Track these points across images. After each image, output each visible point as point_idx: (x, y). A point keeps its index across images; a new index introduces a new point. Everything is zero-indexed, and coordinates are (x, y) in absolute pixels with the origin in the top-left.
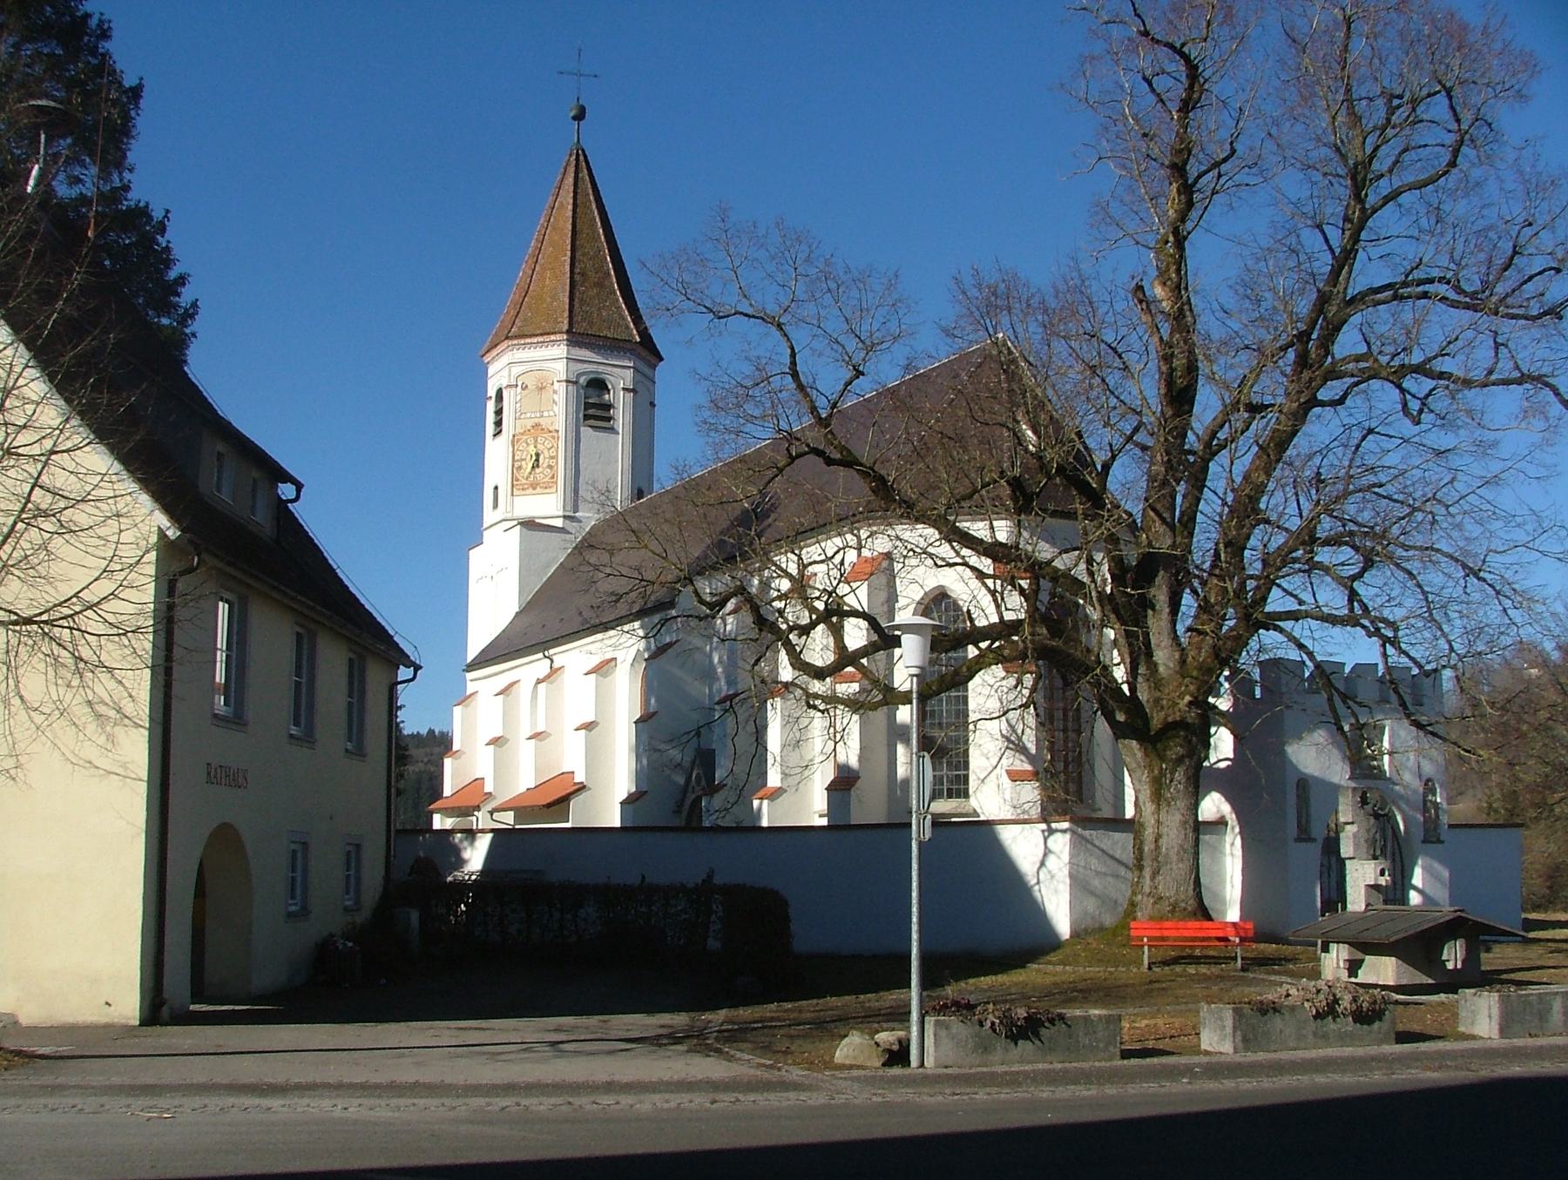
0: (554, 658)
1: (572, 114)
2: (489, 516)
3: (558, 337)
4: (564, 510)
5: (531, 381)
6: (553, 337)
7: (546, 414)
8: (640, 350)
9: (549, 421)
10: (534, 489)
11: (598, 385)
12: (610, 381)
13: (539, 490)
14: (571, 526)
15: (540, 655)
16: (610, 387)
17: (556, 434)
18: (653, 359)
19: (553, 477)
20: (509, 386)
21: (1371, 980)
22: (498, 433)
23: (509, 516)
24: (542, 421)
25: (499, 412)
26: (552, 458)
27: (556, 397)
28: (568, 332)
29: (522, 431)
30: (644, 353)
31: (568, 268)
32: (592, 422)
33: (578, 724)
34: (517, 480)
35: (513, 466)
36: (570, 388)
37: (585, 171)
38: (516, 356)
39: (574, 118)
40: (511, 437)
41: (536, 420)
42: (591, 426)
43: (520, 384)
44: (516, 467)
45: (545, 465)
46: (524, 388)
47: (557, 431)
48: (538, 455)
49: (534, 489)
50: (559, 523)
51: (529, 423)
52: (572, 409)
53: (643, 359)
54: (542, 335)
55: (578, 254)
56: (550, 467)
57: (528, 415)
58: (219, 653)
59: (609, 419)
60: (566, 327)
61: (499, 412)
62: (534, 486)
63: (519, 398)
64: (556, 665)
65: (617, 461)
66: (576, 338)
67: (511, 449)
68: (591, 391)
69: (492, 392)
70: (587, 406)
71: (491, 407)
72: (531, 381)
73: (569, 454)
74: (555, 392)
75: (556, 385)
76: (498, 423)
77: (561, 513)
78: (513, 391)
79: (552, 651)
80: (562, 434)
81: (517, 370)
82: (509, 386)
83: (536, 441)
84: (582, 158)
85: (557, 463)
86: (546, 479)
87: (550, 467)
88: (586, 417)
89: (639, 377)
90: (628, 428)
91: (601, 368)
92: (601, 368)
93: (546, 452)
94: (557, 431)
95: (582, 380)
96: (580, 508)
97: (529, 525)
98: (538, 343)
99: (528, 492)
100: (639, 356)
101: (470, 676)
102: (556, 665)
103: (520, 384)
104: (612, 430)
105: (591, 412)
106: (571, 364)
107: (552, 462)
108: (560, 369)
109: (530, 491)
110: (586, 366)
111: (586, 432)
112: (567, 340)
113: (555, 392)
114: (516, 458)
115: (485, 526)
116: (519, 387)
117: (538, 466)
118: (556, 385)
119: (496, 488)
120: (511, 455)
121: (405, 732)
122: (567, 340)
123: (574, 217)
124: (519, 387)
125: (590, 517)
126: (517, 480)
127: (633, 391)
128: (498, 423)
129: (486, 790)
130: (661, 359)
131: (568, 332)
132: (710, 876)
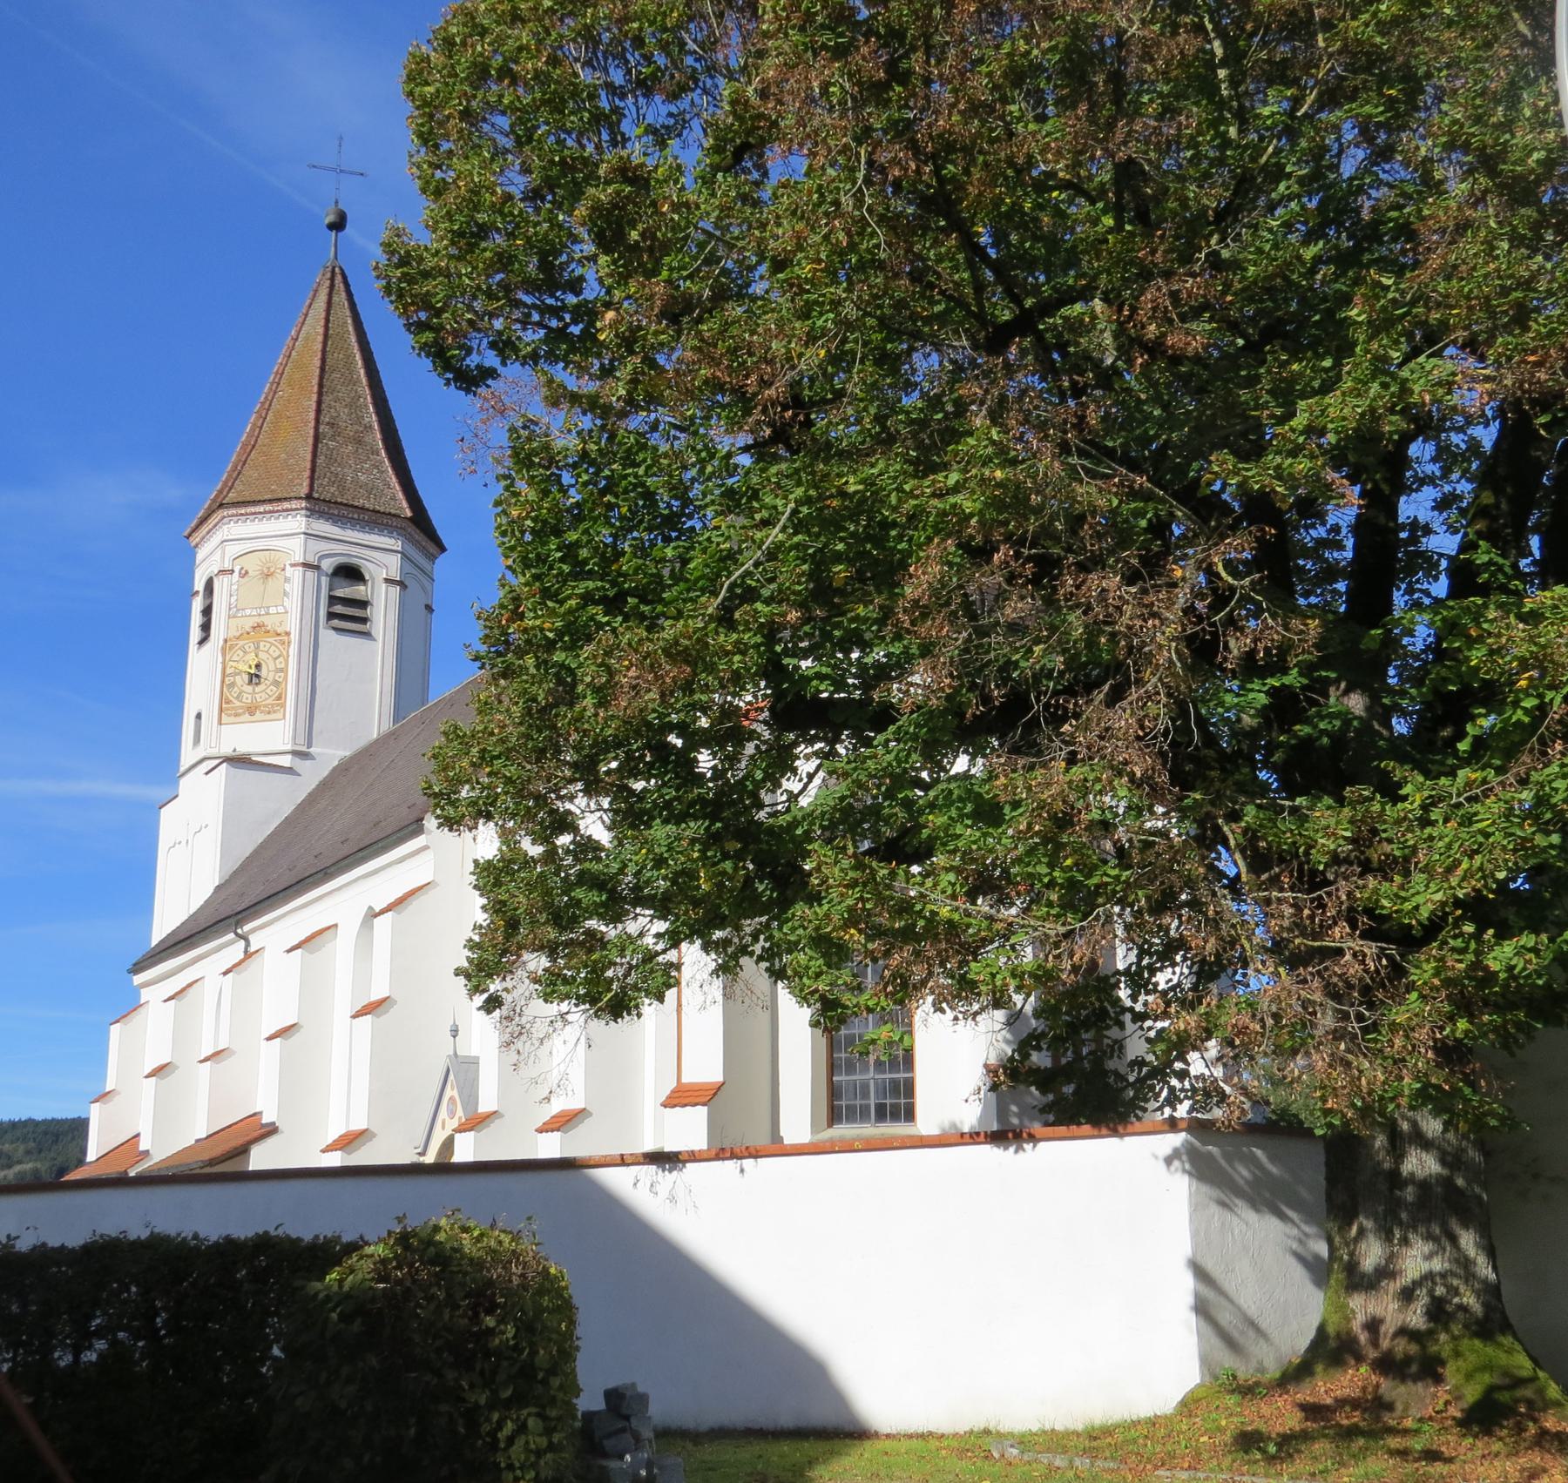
0: (251, 938)
1: (327, 221)
2: (188, 755)
3: (294, 504)
5: (252, 564)
6: (286, 505)
8: (411, 529)
10: (252, 714)
11: (350, 573)
12: (368, 569)
13: (258, 715)
14: (300, 765)
15: (231, 936)
18: (432, 548)
19: (279, 698)
20: (222, 572)
22: (202, 642)
24: (268, 621)
25: (207, 611)
26: (281, 670)
27: (287, 587)
28: (309, 497)
30: (419, 536)
31: (312, 415)
32: (336, 623)
33: (495, 1125)
34: (228, 702)
35: (223, 682)
37: (343, 295)
39: (331, 227)
42: (335, 629)
43: (237, 569)
44: (226, 683)
46: (244, 574)
47: (288, 634)
49: (252, 714)
50: (286, 761)
51: (248, 624)
53: (416, 544)
54: (270, 501)
55: (327, 399)
56: (276, 683)
57: (248, 612)
59: (364, 620)
60: (304, 491)
61: (207, 611)
62: (251, 710)
64: (252, 949)
66: (320, 505)
67: (220, 659)
68: (338, 581)
69: (199, 585)
70: (333, 600)
71: (197, 605)
72: (252, 564)
74: (287, 580)
76: (206, 627)
77: (289, 747)
78: (226, 579)
79: (247, 928)
80: (294, 637)
81: (233, 549)
82: (222, 572)
83: (257, 648)
84: (339, 278)
85: (286, 678)
87: (276, 683)
88: (331, 616)
89: (409, 568)
91: (355, 550)
92: (355, 550)
93: (271, 663)
94: (288, 634)
95: (328, 565)
97: (239, 761)
99: (243, 718)
100: (409, 539)
101: (138, 979)
102: (252, 949)
103: (237, 569)
104: (367, 635)
105: (339, 609)
106: (312, 543)
107: (279, 677)
108: (296, 549)
109: (247, 717)
111: (328, 637)
113: (287, 580)
114: (229, 671)
115: (182, 769)
116: (236, 574)
119: (199, 716)
120: (220, 666)
121: (705, 1147)
123: (324, 351)
124: (236, 574)
125: (330, 754)
127: (401, 584)
128: (206, 627)
129: (142, 1148)
130: (443, 549)
131: (309, 497)
132: (458, 972)
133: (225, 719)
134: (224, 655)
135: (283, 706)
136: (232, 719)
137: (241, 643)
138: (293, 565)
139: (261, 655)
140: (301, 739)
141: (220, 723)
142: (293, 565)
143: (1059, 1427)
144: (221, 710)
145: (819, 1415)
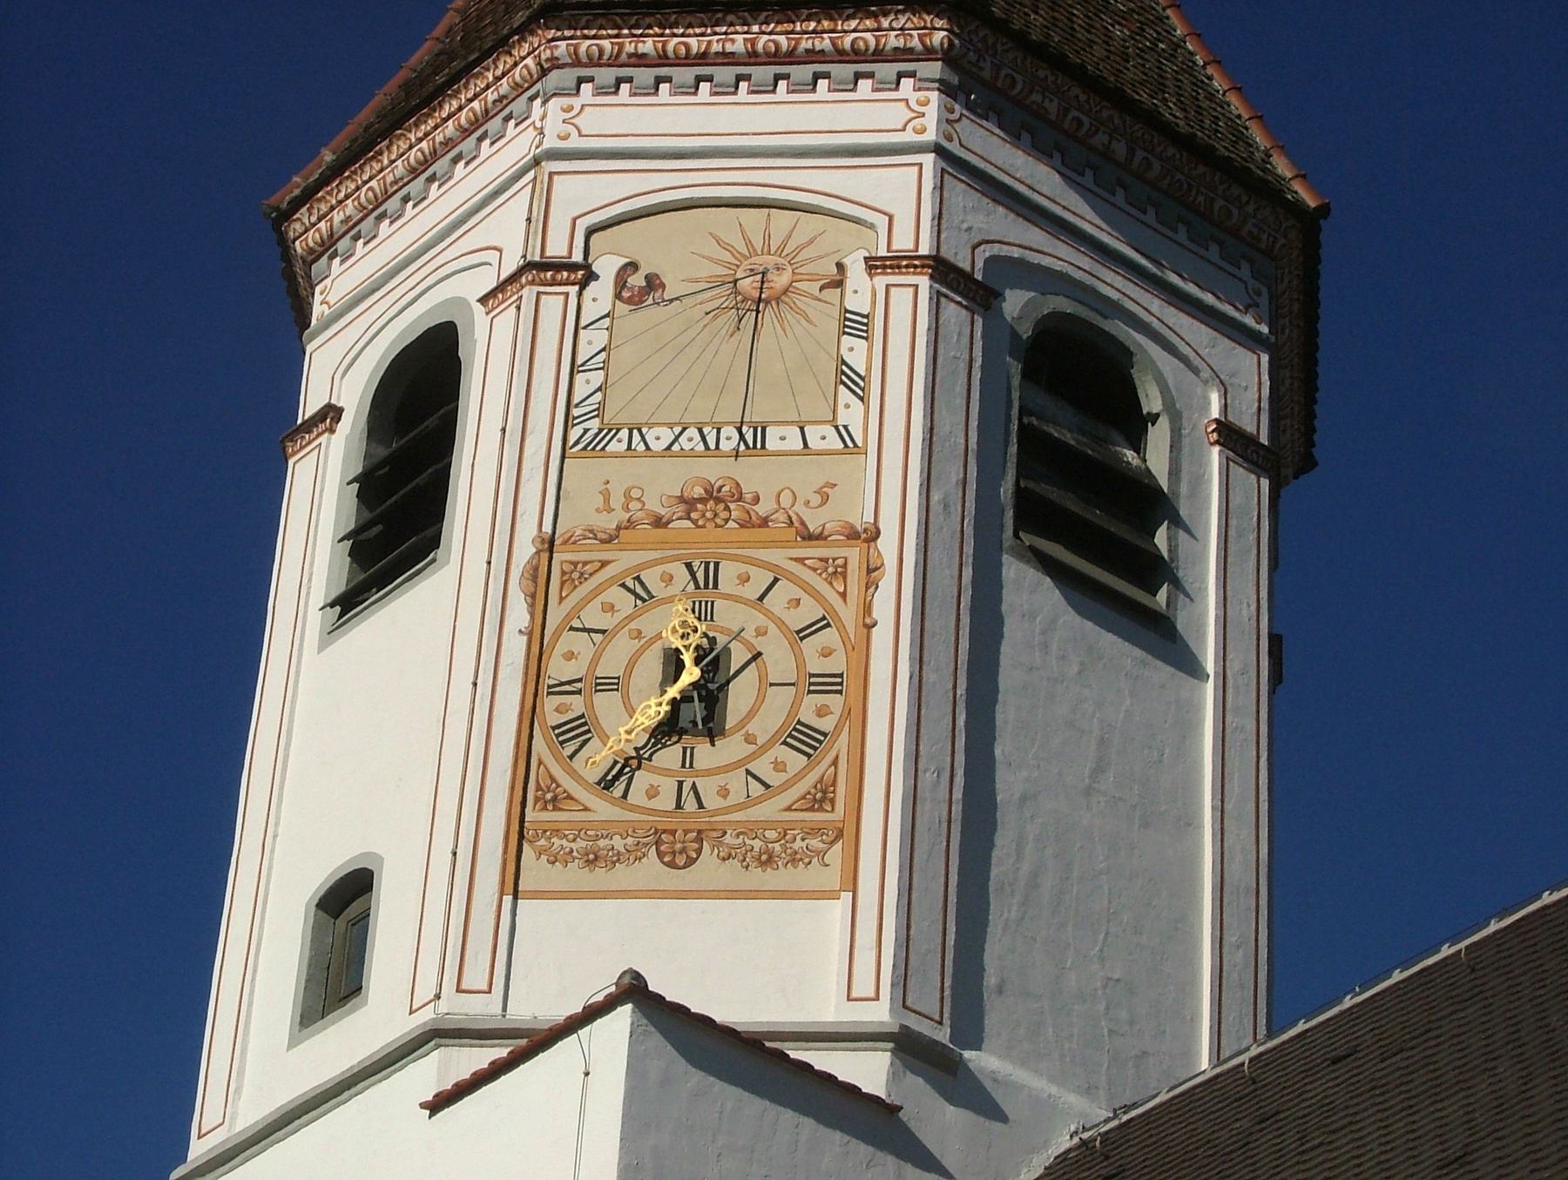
4: (902, 1003)
7: (781, 438)
9: (807, 477)
13: (709, 868)
16: (1151, 401)
17: (854, 554)
19: (821, 797)
21: (196, 1156)
23: (482, 1009)
24: (753, 476)
26: (829, 684)
29: (608, 523)
34: (556, 801)
35: (530, 714)
36: (954, 313)
38: (588, 121)
40: (525, 550)
41: (714, 471)
43: (607, 267)
45: (770, 721)
48: (713, 660)
52: (960, 431)
56: (805, 738)
58: (1123, 1121)
63: (593, 340)
65: (1189, 822)
67: (519, 615)
73: (938, 679)
74: (855, 324)
75: (861, 291)
77: (880, 1014)
85: (858, 717)
86: (770, 810)
87: (805, 738)
90: (1251, 660)
91: (1113, 284)
92: (1113, 284)
96: (991, 1021)
98: (753, 58)
99: (623, 876)
106: (961, 195)
110: (1036, 236)
112: (948, 57)
113: (855, 324)
114: (558, 669)
116: (600, 295)
117: (712, 729)
118: (861, 291)
120: (515, 648)
122: (948, 57)
124: (600, 295)
126: (556, 801)
133: (534, 870)
134: (539, 602)
135: (847, 834)
136: (575, 875)
137: (624, 561)
138: (874, 265)
139: (729, 616)
140: (928, 997)
141: (512, 887)
142: (874, 265)
143: (998, 814)
144: (519, 834)
145: (663, 1052)
